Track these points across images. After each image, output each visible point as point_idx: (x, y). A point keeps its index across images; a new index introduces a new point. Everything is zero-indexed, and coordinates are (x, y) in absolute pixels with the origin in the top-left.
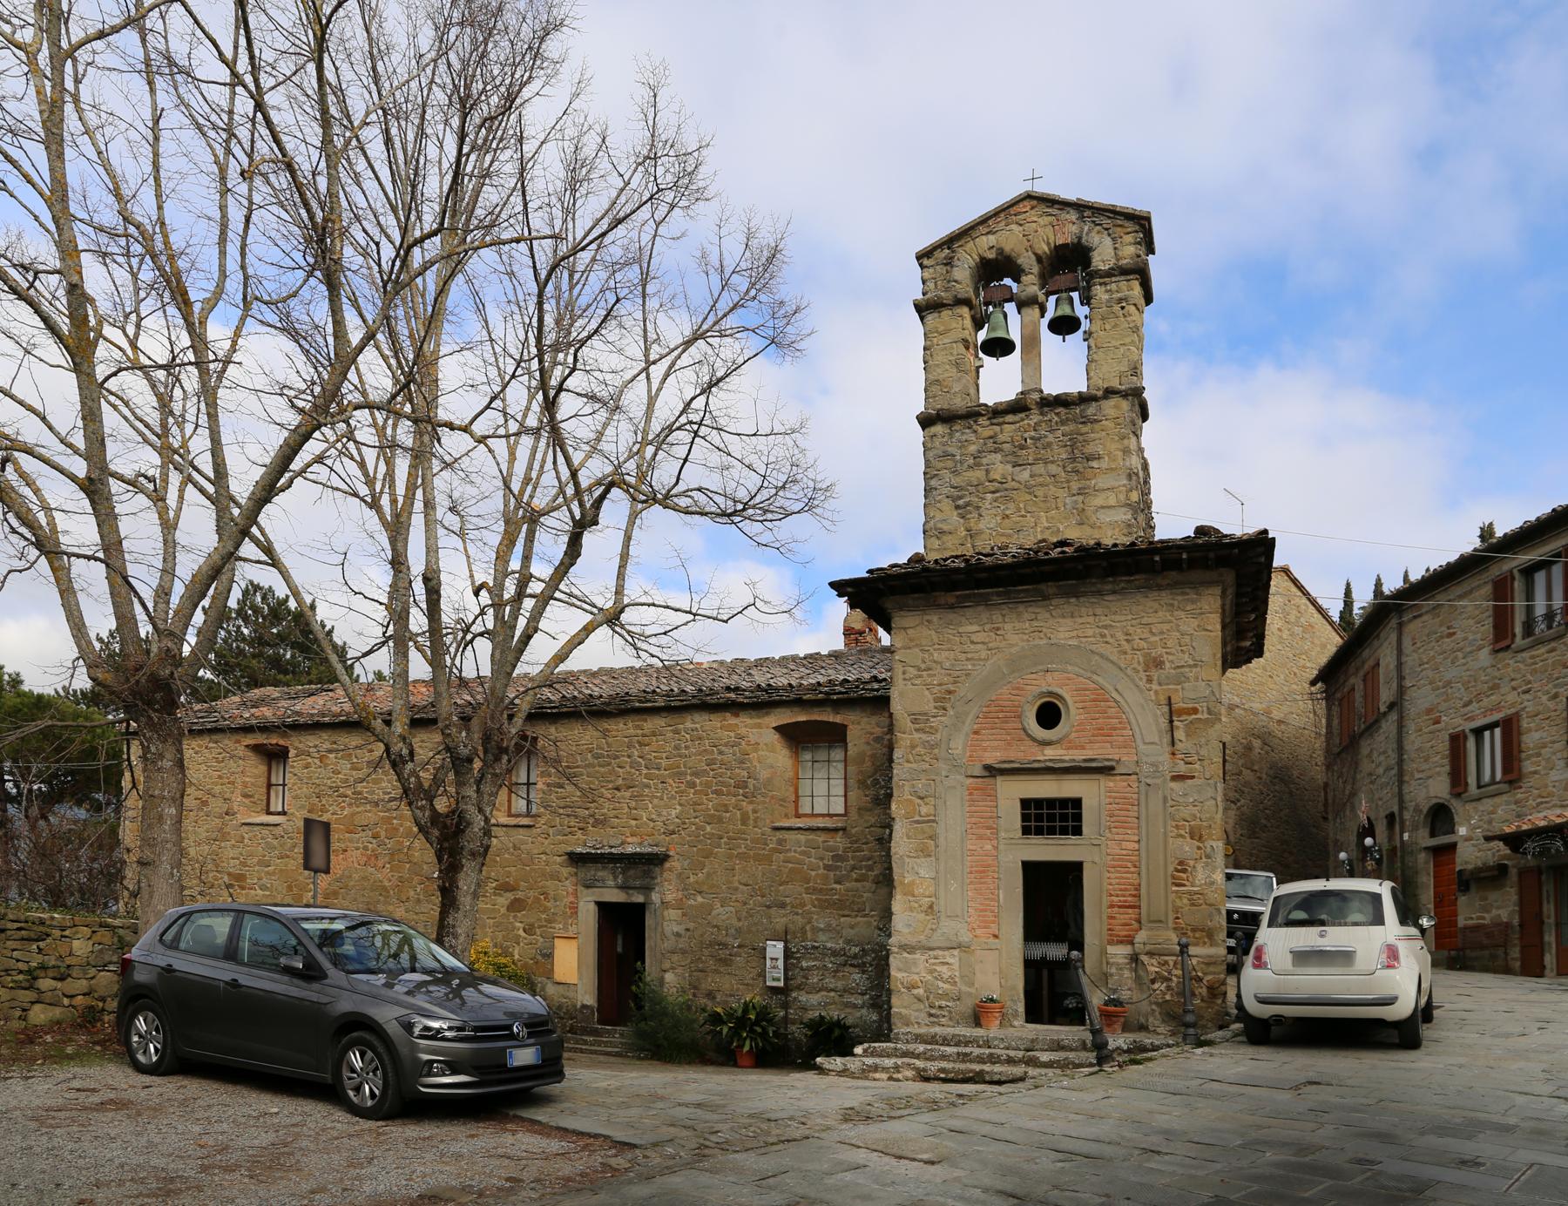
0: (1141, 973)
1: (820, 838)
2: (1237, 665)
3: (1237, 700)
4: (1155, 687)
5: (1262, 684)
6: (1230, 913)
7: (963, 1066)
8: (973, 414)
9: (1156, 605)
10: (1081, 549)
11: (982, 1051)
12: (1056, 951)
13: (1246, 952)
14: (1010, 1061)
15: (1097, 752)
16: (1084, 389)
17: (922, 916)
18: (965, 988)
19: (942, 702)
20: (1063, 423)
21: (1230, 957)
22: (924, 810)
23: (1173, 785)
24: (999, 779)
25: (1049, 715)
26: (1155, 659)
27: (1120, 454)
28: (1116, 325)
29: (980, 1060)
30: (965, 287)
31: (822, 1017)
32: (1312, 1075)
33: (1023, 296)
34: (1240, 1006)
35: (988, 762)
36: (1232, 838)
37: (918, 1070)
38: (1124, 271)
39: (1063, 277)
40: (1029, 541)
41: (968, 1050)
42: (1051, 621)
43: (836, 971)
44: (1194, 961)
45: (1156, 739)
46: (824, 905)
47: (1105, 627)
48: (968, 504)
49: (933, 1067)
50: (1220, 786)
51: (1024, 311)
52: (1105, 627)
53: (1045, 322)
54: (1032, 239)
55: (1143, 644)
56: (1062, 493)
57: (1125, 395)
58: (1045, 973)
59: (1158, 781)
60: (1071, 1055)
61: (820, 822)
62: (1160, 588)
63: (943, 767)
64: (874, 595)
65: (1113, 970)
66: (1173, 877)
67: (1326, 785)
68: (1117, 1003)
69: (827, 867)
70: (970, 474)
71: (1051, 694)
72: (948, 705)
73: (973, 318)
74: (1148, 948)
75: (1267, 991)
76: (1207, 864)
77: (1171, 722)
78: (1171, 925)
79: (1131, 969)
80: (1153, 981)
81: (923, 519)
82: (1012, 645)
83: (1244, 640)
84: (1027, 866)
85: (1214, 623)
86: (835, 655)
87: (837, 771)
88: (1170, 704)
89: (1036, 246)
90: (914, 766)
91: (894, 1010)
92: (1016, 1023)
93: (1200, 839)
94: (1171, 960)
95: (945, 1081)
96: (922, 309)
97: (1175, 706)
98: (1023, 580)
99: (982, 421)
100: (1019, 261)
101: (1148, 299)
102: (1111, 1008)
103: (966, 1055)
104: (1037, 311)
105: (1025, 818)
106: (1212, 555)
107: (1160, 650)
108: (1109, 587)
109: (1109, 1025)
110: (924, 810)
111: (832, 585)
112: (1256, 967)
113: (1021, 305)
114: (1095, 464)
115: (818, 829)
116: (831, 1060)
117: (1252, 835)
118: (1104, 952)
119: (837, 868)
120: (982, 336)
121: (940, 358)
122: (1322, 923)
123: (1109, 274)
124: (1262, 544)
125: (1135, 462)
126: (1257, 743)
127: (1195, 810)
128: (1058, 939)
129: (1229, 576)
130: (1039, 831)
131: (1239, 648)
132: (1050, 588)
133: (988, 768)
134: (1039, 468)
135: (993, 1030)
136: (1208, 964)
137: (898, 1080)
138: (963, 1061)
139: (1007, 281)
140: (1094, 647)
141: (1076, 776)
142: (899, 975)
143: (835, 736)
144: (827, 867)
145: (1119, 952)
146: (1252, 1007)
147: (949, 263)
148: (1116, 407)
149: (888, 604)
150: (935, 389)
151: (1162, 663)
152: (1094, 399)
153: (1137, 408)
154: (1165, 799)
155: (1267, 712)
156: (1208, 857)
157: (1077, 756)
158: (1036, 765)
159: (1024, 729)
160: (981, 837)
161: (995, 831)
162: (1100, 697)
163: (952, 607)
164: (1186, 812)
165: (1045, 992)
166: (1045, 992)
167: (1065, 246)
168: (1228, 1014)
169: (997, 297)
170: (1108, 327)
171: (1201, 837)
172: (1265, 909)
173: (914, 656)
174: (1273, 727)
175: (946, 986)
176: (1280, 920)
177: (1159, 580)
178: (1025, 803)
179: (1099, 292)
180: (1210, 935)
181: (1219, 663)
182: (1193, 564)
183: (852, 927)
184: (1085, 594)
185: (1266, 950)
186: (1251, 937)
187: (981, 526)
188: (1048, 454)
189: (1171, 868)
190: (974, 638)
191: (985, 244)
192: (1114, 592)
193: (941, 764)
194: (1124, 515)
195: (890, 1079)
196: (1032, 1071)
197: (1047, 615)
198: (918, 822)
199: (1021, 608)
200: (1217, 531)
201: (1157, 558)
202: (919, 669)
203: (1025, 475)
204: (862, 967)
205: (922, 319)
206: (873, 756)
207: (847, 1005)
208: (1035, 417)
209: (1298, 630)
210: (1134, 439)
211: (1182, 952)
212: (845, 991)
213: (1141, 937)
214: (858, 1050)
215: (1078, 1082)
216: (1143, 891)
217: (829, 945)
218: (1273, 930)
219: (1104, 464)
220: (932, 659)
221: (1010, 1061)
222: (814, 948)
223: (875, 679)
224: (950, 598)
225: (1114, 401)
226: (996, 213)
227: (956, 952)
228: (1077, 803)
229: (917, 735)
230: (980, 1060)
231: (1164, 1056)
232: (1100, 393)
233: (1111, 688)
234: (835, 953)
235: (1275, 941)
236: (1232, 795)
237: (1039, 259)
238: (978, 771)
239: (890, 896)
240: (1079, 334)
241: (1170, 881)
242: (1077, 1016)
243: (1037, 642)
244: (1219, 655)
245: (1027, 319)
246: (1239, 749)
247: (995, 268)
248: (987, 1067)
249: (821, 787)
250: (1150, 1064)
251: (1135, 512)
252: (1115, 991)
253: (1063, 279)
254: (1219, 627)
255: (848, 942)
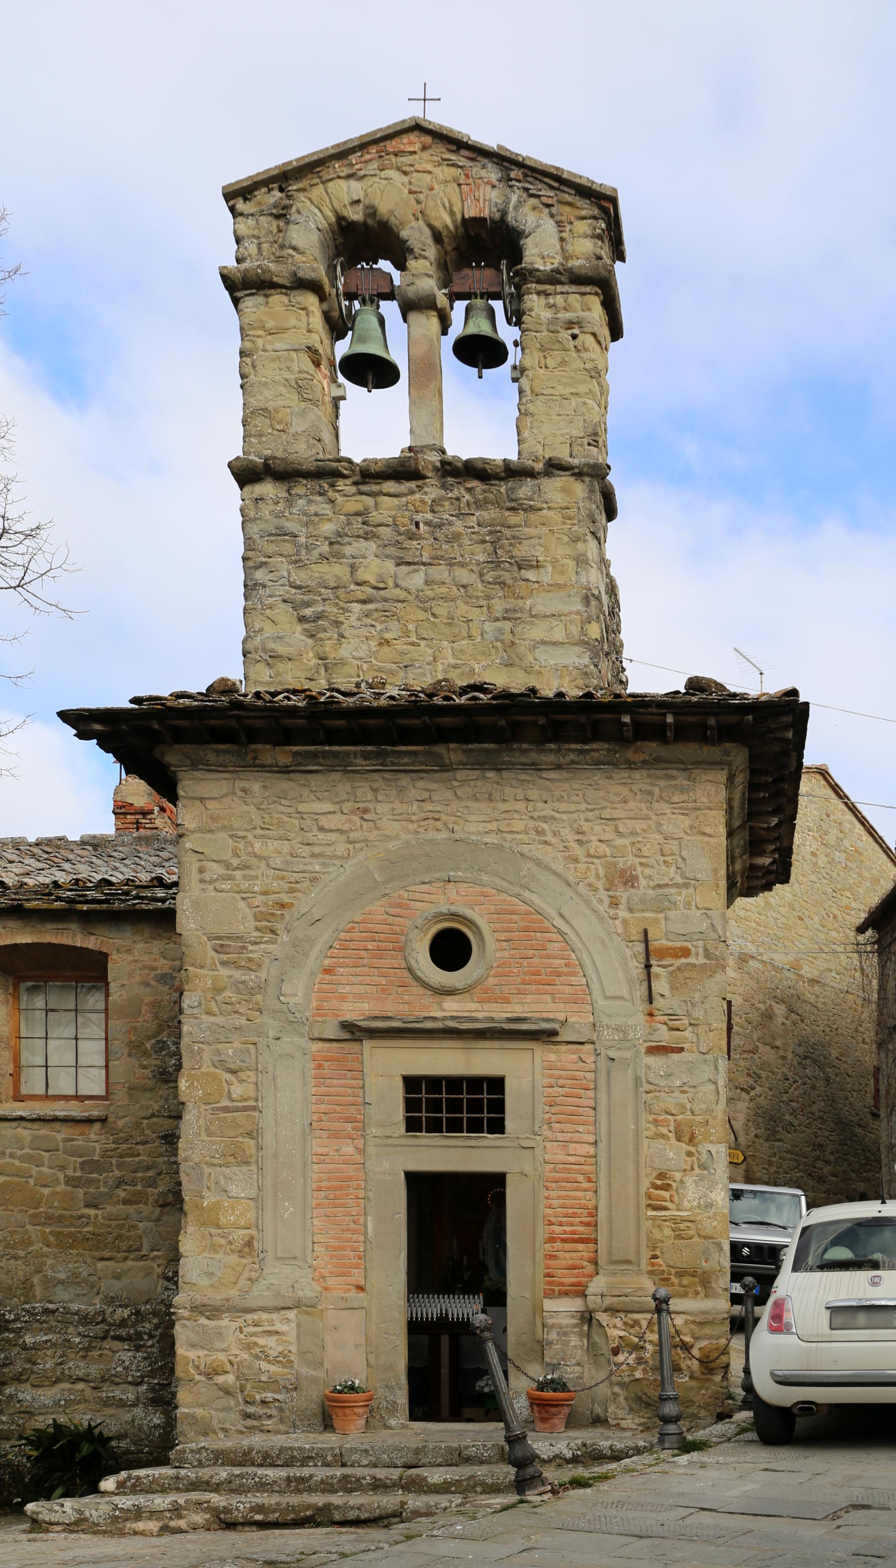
0: (597, 1339)
1: (60, 1134)
2: (750, 892)
3: (751, 949)
4: (623, 913)
5: (787, 928)
6: (736, 1247)
7: (294, 1500)
8: (328, 473)
9: (625, 791)
10: (506, 695)
11: (329, 1471)
12: (466, 1308)
13: (761, 1300)
14: (378, 1486)
15: (533, 1007)
16: (513, 456)
17: (233, 1259)
18: (305, 1371)
19: (270, 920)
20: (480, 505)
21: (737, 1309)
22: (237, 1090)
23: (651, 1060)
24: (367, 1044)
25: (451, 949)
26: (622, 873)
27: (571, 564)
28: (563, 363)
29: (327, 1487)
30: (313, 264)
31: (56, 1425)
32: (858, 1494)
33: (411, 292)
34: (748, 1387)
35: (350, 1017)
36: (742, 1139)
37: (215, 1512)
38: (578, 279)
39: (477, 273)
40: (421, 680)
41: (306, 1472)
42: (454, 806)
43: (88, 1349)
44: (679, 1321)
45: (625, 993)
46: (65, 1243)
47: (544, 819)
48: (319, 617)
49: (241, 1504)
50: (723, 1064)
51: (413, 316)
52: (544, 819)
53: (447, 342)
54: (424, 200)
55: (604, 849)
56: (475, 614)
57: (579, 474)
58: (445, 1340)
59: (628, 1054)
60: (480, 1471)
61: (60, 1109)
62: (631, 765)
63: (272, 1025)
64: (147, 739)
65: (553, 1336)
66: (649, 1197)
67: (877, 1069)
68: (559, 1385)
69: (69, 1181)
70: (324, 568)
71: (454, 916)
72: (278, 926)
73: (327, 317)
74: (608, 1301)
75: (790, 1366)
76: (701, 1178)
77: (648, 966)
78: (644, 1265)
79: (581, 1335)
80: (616, 1352)
81: (243, 633)
82: (389, 838)
83: (761, 855)
84: (414, 1180)
85: (716, 825)
86: (94, 845)
87: (94, 1027)
88: (646, 941)
89: (432, 214)
90: (220, 1020)
91: (182, 1411)
92: (393, 1422)
93: (691, 1140)
94: (644, 1319)
95: (263, 1525)
96: (237, 286)
97: (653, 945)
98: (405, 736)
99: (341, 484)
100: (404, 234)
101: (616, 332)
102: (549, 1394)
103: (302, 1480)
104: (434, 322)
105: (411, 1105)
106: (712, 721)
107: (631, 860)
108: (551, 758)
109: (544, 1420)
110: (237, 1090)
111: (65, 716)
112: (773, 1330)
113: (408, 308)
114: (531, 575)
115: (56, 1119)
116: (54, 1504)
117: (772, 1136)
118: (538, 1309)
119: (90, 1182)
120: (342, 348)
121: (267, 372)
122: (875, 1265)
123: (552, 278)
124: (786, 716)
125: (594, 578)
126: (780, 1010)
127: (683, 1099)
128: (468, 1289)
129: (739, 757)
130: (434, 1127)
131: (753, 867)
132: (452, 753)
133: (347, 1026)
134: (440, 572)
135: (353, 1436)
136: (701, 1324)
137: (180, 1531)
138: (298, 1491)
139: (385, 265)
140: (525, 849)
141: (496, 1044)
142: (192, 1354)
143: (90, 970)
144: (69, 1181)
145: (562, 1309)
146: (767, 1390)
147: (281, 215)
148: (565, 490)
149: (172, 757)
150: (260, 423)
151: (636, 878)
152: (531, 474)
153: (598, 496)
154: (637, 1081)
155: (795, 968)
156: (703, 1167)
157: (497, 1013)
158: (429, 1025)
159: (410, 970)
160: (336, 1135)
161: (362, 1128)
162: (533, 929)
163: (285, 771)
164: (670, 1101)
165: (445, 1371)
166: (445, 1371)
167: (478, 222)
168: (730, 1397)
169: (368, 287)
170: (550, 363)
171: (691, 1140)
172: (790, 1241)
173: (219, 844)
174: (804, 988)
175: (274, 1369)
176: (811, 1261)
177: (630, 754)
178: (411, 1083)
179: (534, 303)
180: (705, 1281)
181: (723, 884)
182: (682, 734)
183: (118, 1277)
184: (510, 766)
185: (788, 1305)
186: (767, 1281)
187: (344, 652)
188: (454, 551)
189: (646, 1183)
190: (324, 822)
191: (344, 195)
192: (558, 767)
193: (267, 1019)
194: (578, 658)
195: (165, 1530)
196: (415, 1502)
197: (449, 795)
198: (226, 1109)
199: (405, 780)
200: (720, 687)
201: (626, 719)
202: (228, 867)
203: (416, 579)
204: (135, 1341)
205: (236, 302)
206: (156, 1005)
207: (107, 1402)
208: (432, 491)
209: (839, 856)
210: (593, 544)
211: (658, 1310)
212: (103, 1380)
213: (597, 1285)
214: (108, 1484)
215: (483, 1523)
216: (602, 1217)
217: (75, 1307)
218: (802, 1276)
219: (546, 576)
220: (261, 856)
221: (378, 1486)
222: (46, 1311)
223: (159, 882)
224: (282, 755)
225: (561, 481)
226: (363, 145)
227: (291, 1315)
228: (497, 1084)
229: (224, 972)
230: (327, 1487)
231: (628, 1471)
232: (539, 466)
233: (553, 913)
234: (85, 1320)
235: (801, 1291)
236: (743, 1080)
237: (437, 237)
238: (332, 1031)
239: (177, 1230)
240: (505, 369)
241: (644, 1202)
242: (489, 1407)
243: (431, 835)
244: (723, 872)
245: (418, 332)
246: (755, 1017)
247: (363, 241)
248: (336, 1499)
249: (60, 1052)
250: (604, 1486)
251: (594, 655)
252: (554, 1367)
253: (478, 277)
254: (722, 830)
255: (111, 1300)
